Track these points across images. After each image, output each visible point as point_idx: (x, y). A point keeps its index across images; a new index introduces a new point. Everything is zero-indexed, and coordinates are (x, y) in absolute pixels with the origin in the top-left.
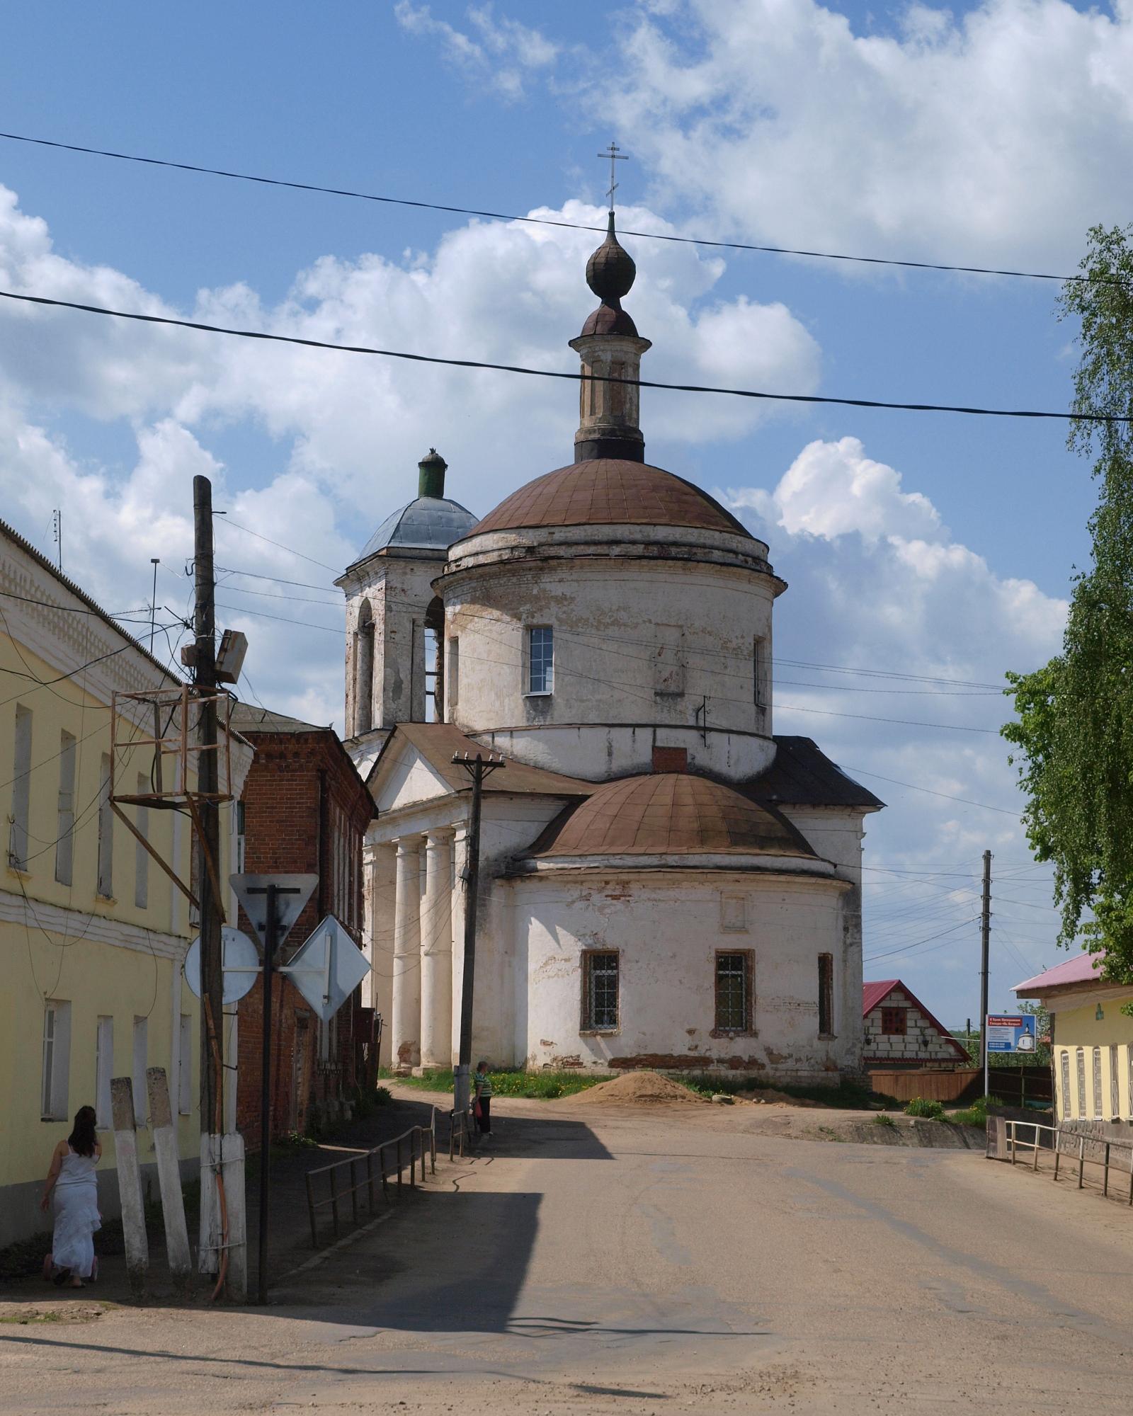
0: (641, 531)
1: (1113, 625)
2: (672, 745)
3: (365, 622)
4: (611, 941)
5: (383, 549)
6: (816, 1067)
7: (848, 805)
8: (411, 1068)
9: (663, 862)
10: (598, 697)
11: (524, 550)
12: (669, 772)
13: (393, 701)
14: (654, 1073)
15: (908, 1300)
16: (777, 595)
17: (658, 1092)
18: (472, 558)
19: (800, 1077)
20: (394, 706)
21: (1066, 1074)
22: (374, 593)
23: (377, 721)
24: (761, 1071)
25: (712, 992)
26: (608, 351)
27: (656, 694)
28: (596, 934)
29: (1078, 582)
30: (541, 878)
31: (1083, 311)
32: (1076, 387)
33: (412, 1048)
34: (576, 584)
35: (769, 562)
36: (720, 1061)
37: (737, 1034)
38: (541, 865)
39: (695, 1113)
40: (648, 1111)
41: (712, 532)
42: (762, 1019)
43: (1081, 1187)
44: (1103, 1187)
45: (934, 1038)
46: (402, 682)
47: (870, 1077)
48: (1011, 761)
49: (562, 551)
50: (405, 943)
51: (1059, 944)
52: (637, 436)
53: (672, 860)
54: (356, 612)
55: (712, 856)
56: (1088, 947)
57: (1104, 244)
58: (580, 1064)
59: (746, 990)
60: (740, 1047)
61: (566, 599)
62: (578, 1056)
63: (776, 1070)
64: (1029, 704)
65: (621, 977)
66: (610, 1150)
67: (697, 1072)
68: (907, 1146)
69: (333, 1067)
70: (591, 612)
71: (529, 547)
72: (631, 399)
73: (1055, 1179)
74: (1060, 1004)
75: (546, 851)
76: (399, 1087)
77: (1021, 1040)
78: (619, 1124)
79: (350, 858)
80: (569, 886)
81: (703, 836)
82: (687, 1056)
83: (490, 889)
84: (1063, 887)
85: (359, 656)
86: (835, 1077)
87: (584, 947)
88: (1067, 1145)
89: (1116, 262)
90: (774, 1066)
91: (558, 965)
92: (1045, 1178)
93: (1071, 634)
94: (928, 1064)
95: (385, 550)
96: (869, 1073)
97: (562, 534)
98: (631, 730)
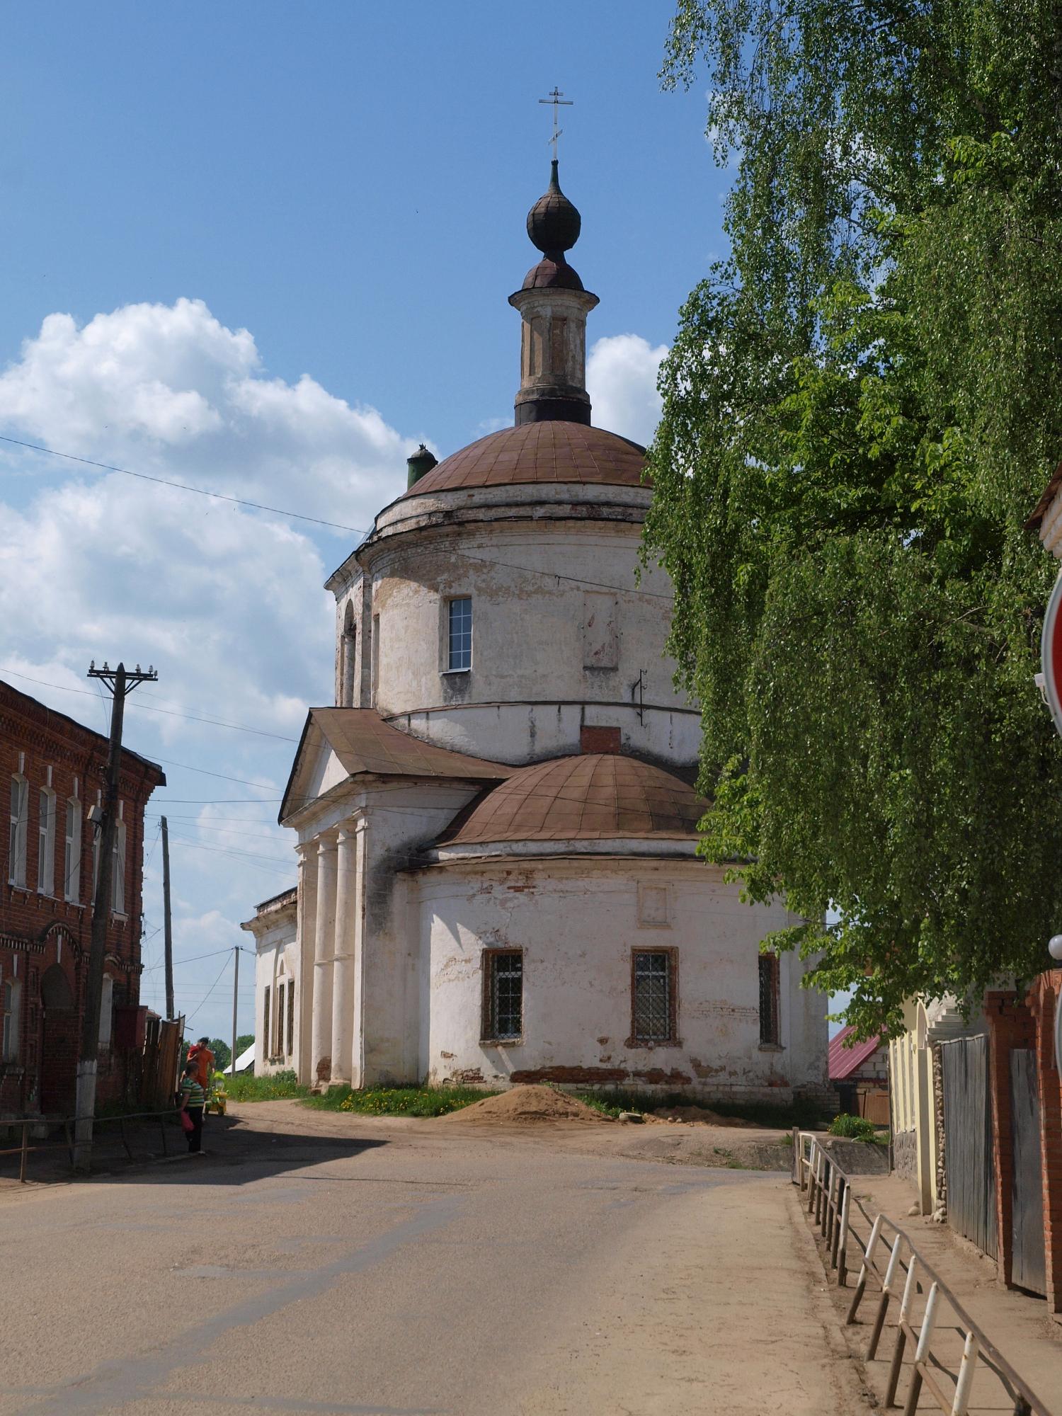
0: (568, 491)
2: (603, 724)
4: (514, 940)
6: (757, 1082)
9: (571, 848)
10: (520, 672)
11: (441, 515)
17: (542, 1107)
19: (735, 1093)
21: (896, 1078)
24: (686, 1086)
25: (628, 996)
26: (548, 307)
27: (585, 668)
30: (441, 869)
34: (495, 549)
36: (637, 1074)
38: (443, 855)
40: (520, 1130)
42: (687, 1027)
49: (481, 514)
52: (580, 396)
53: (581, 846)
55: (627, 841)
58: (480, 1079)
60: (661, 1058)
62: (479, 1069)
63: (705, 1084)
67: (610, 1087)
70: (513, 580)
71: (447, 512)
72: (574, 357)
80: (469, 877)
81: (622, 818)
82: (598, 1069)
83: (391, 885)
87: (485, 946)
90: (703, 1080)
97: (482, 496)
98: (555, 708)
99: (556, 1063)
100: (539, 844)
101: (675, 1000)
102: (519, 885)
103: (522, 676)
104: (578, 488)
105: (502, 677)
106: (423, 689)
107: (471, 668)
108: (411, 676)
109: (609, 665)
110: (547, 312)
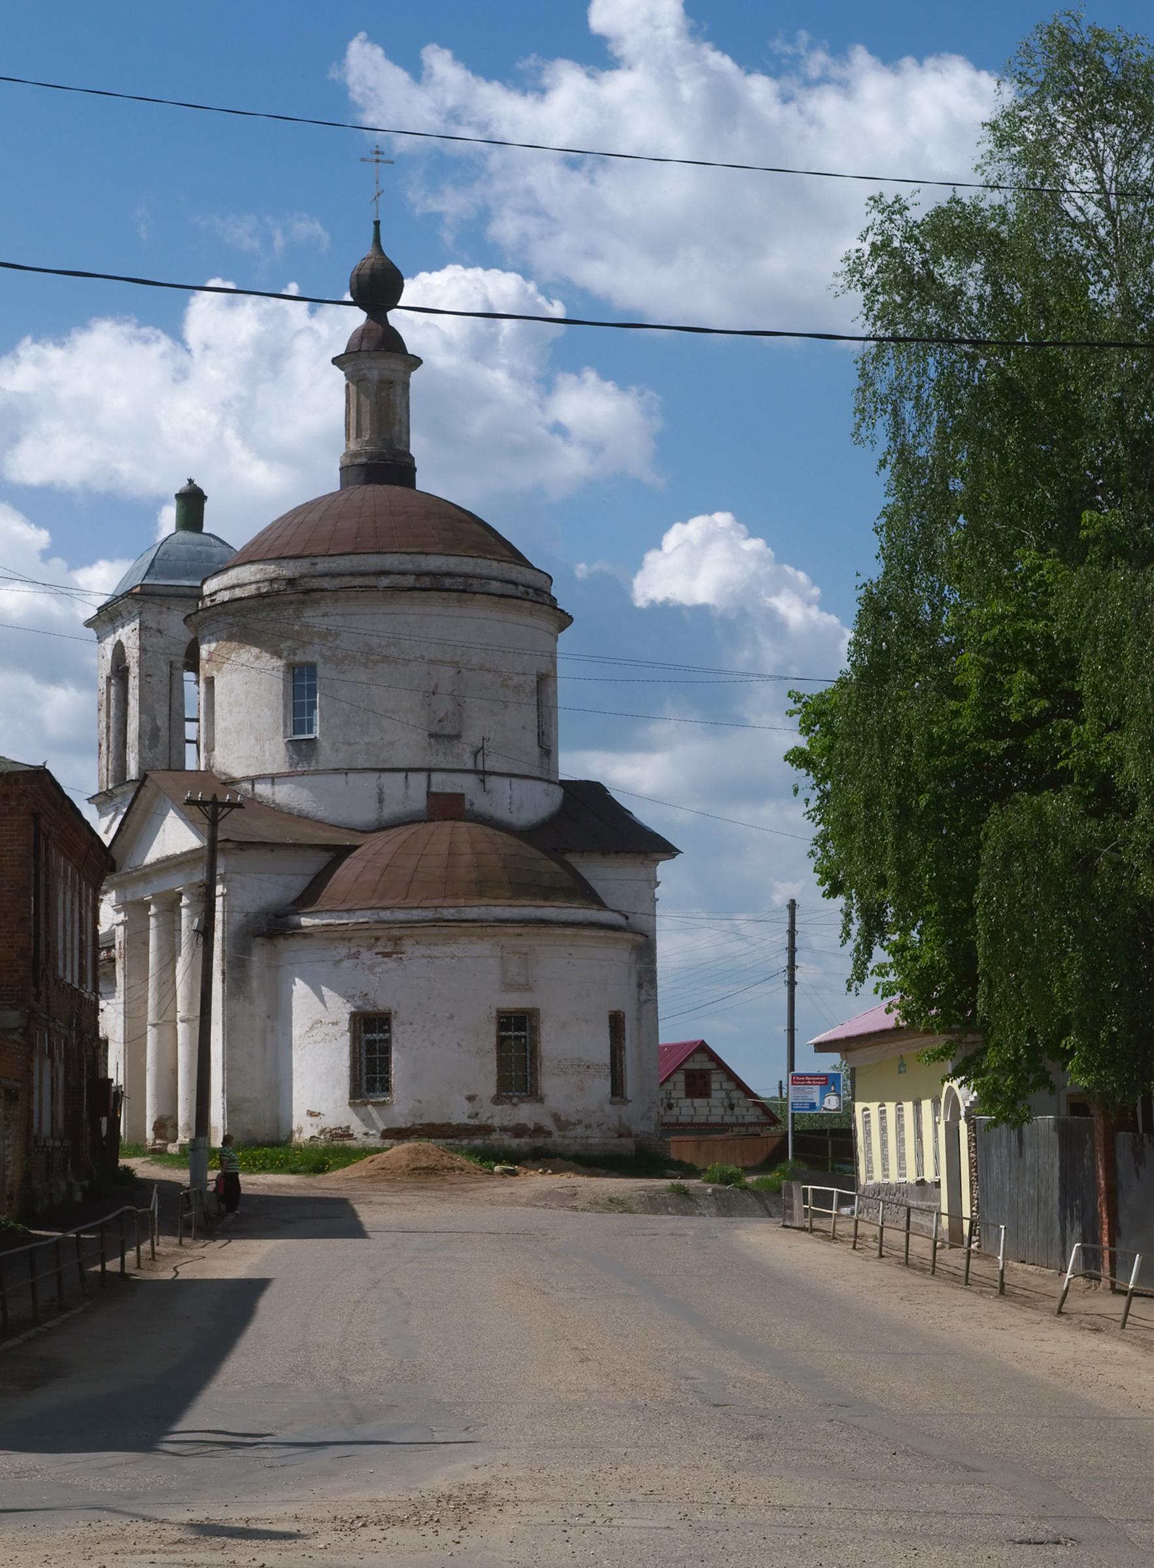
1: (903, 634)
2: (449, 790)
3: (118, 667)
4: (383, 1003)
5: (137, 586)
7: (640, 853)
8: (166, 1145)
9: (438, 916)
10: (367, 740)
11: (284, 583)
12: (446, 820)
13: (150, 749)
14: (430, 1144)
15: (658, 1394)
16: (561, 629)
17: (432, 1163)
18: (228, 592)
19: (591, 1144)
20: (151, 755)
21: (868, 1133)
22: (128, 634)
23: (133, 771)
24: (548, 1140)
25: (493, 1056)
26: (375, 370)
27: (431, 736)
28: (366, 995)
29: (864, 588)
30: (305, 936)
31: (864, 288)
32: (859, 372)
33: (169, 1123)
35: (553, 594)
36: (503, 1129)
37: (522, 1100)
38: (305, 921)
39: (472, 1186)
40: (420, 1185)
41: (489, 562)
42: (550, 1084)
43: (881, 1256)
44: (903, 1255)
45: (740, 1101)
46: (158, 729)
47: (669, 1143)
48: (796, 791)
49: (325, 583)
50: (159, 1003)
51: (849, 989)
52: (407, 460)
53: (448, 913)
54: (109, 655)
55: (492, 908)
56: (880, 991)
57: (885, 214)
58: (350, 1136)
59: (531, 1052)
60: (525, 1113)
61: (330, 635)
62: (348, 1127)
64: (815, 726)
65: (393, 1040)
66: (367, 1228)
67: (478, 1142)
68: (705, 1216)
69: (58, 1144)
72: (400, 420)
73: (854, 1248)
74: (862, 1056)
75: (311, 905)
76: (152, 1165)
77: (826, 1099)
78: (386, 1199)
79: (80, 914)
81: (482, 888)
82: (466, 1125)
84: (851, 926)
85: (113, 703)
86: (628, 1144)
87: (353, 1009)
88: (870, 1210)
89: (899, 234)
90: (563, 1133)
91: (324, 1030)
92: (844, 1247)
93: (856, 645)
94: (735, 1129)
95: (139, 588)
96: (667, 1140)
97: (326, 565)
98: (403, 775)
99: (425, 1121)
100: (407, 911)
101: (536, 1059)
102: (386, 950)
103: (369, 743)
104: (421, 558)
105: (350, 744)
106: (267, 754)
107: (318, 735)
108: (253, 741)
109: (452, 733)
110: (374, 375)
